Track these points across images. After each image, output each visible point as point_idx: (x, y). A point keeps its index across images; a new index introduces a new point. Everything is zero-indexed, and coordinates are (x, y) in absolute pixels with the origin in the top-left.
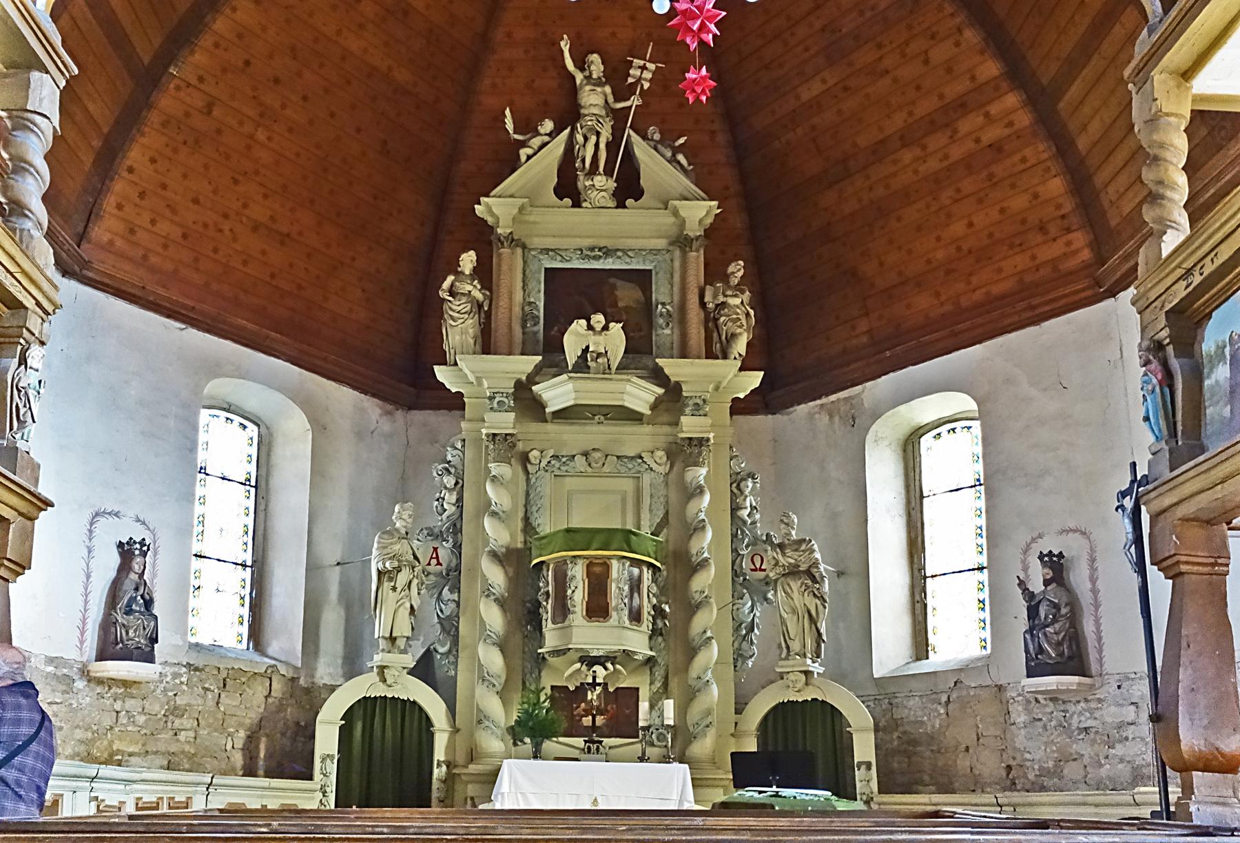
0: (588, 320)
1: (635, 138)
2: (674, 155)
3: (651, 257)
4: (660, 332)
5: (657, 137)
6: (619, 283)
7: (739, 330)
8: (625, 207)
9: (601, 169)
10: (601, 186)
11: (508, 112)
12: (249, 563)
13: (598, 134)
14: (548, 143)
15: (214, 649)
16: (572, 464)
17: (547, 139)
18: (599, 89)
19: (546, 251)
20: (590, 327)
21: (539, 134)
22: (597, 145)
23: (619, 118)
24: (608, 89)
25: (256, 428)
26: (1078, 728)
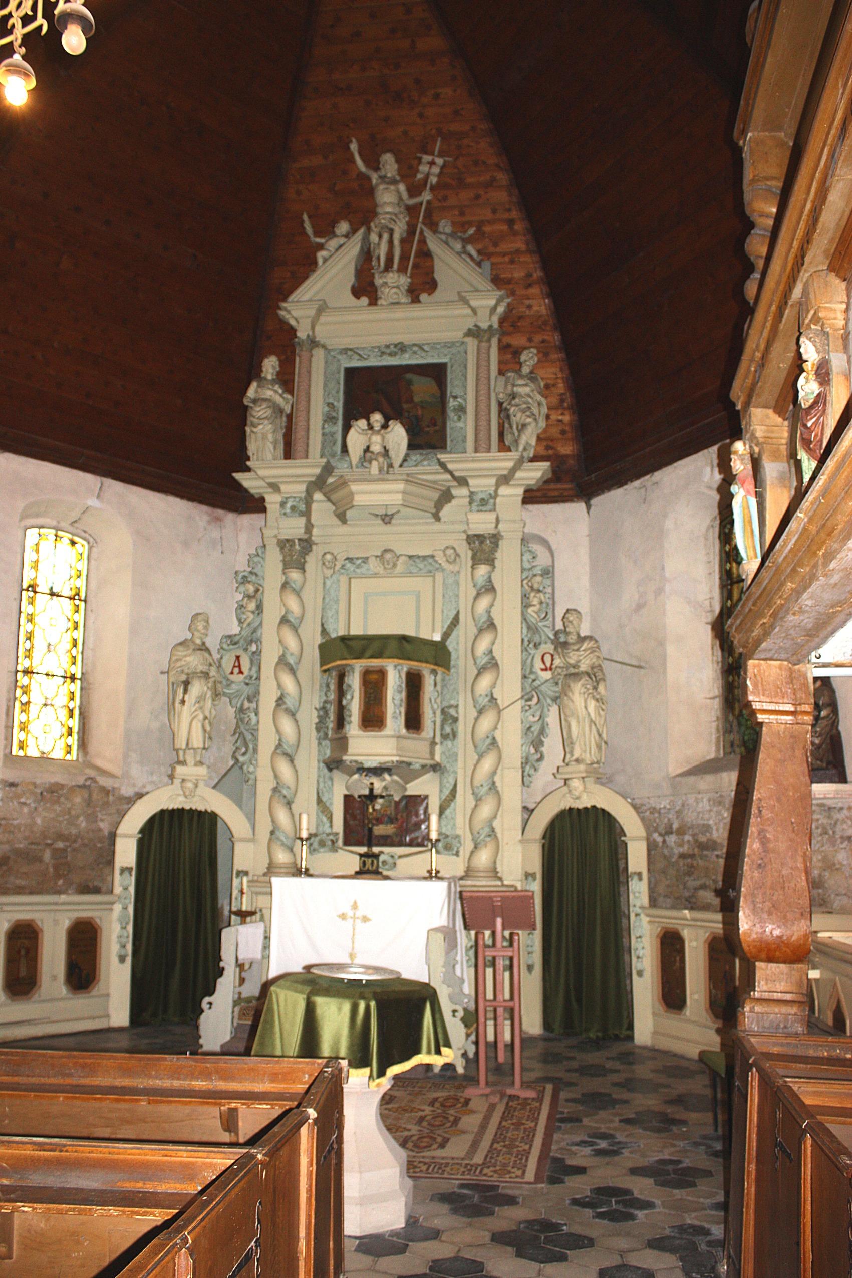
0: (368, 420)
1: (428, 234)
2: (464, 247)
3: (446, 351)
4: (453, 425)
5: (448, 230)
6: (415, 378)
7: (529, 420)
8: (419, 301)
9: (395, 266)
10: (393, 283)
11: (305, 217)
12: (78, 676)
13: (391, 232)
14: (344, 244)
15: (44, 760)
16: (365, 566)
17: (342, 241)
18: (392, 187)
19: (345, 351)
20: (370, 427)
21: (334, 235)
22: (391, 242)
23: (412, 211)
24: (402, 187)
25: (85, 543)
26: (842, 837)
